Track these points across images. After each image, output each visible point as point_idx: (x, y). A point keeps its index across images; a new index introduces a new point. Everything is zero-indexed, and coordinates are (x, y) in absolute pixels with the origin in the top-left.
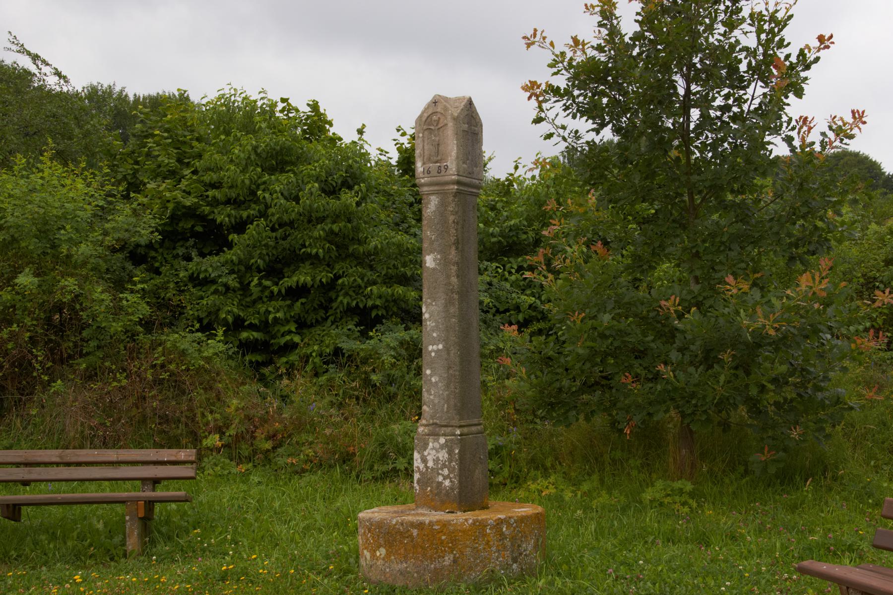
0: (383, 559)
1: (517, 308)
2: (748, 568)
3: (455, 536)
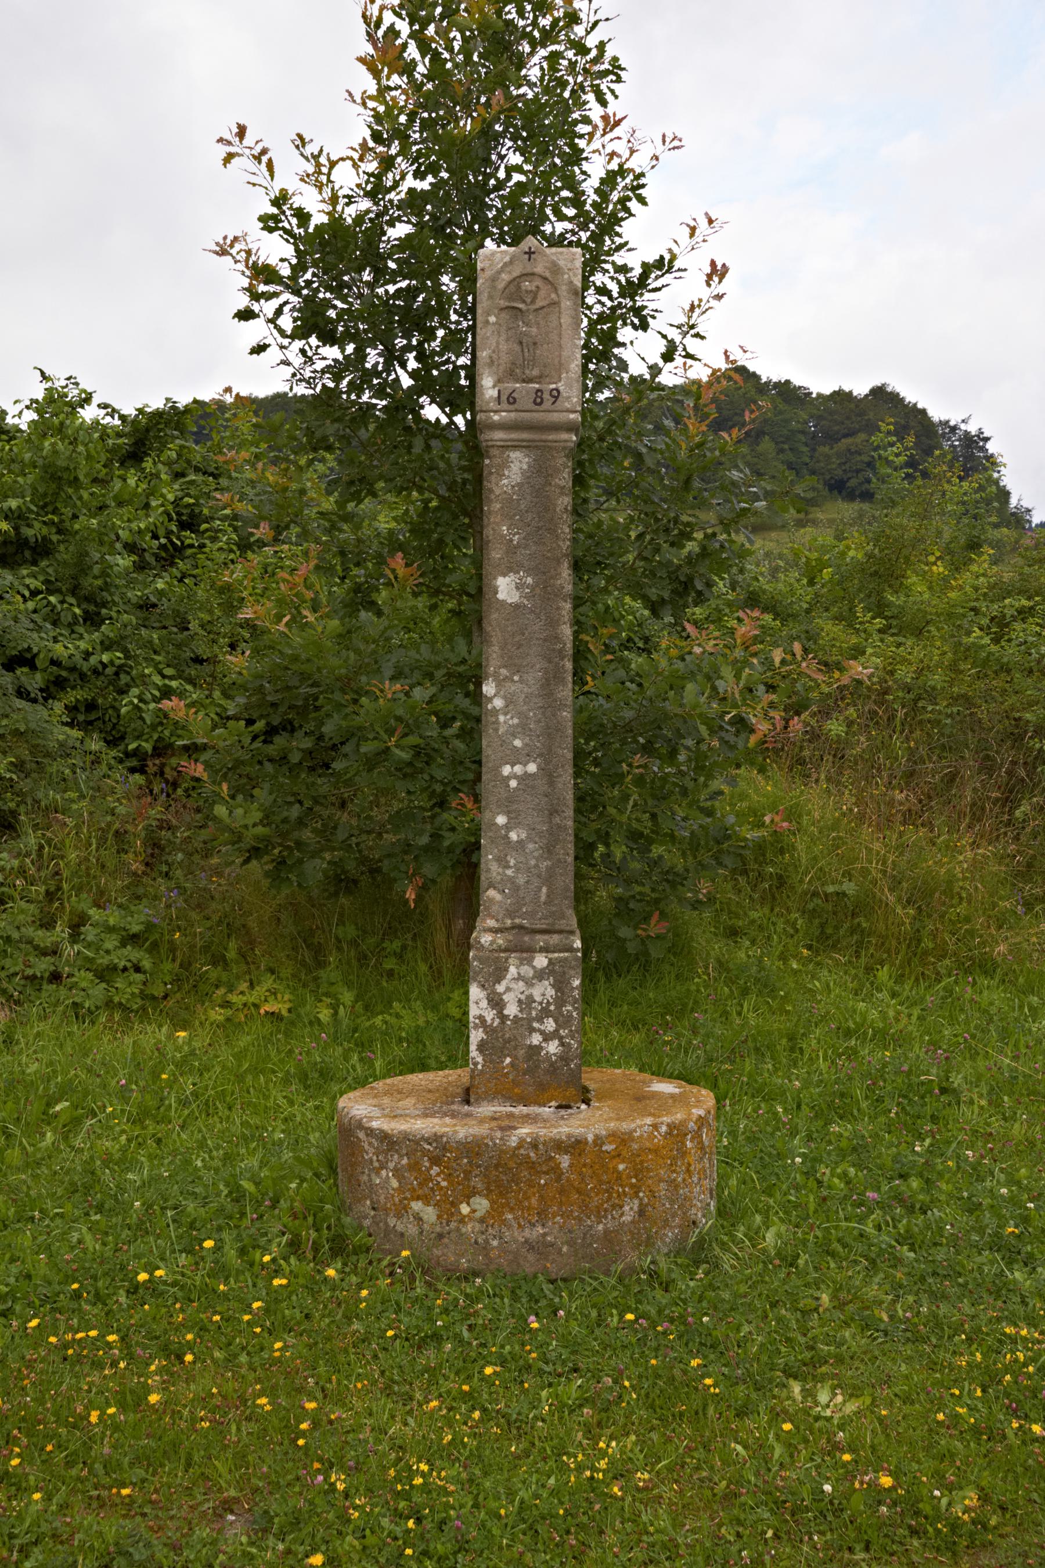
3: (642, 1162)
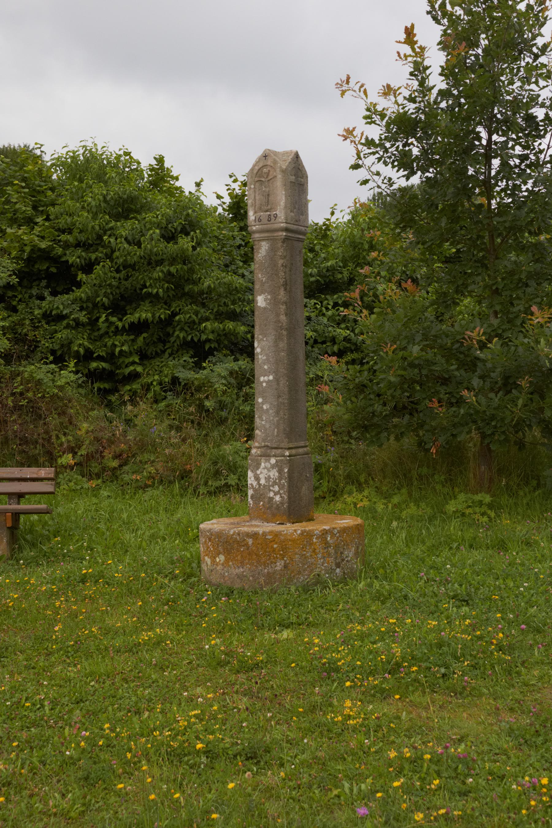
0: (223, 565)
1: (333, 340)
2: (542, 571)
